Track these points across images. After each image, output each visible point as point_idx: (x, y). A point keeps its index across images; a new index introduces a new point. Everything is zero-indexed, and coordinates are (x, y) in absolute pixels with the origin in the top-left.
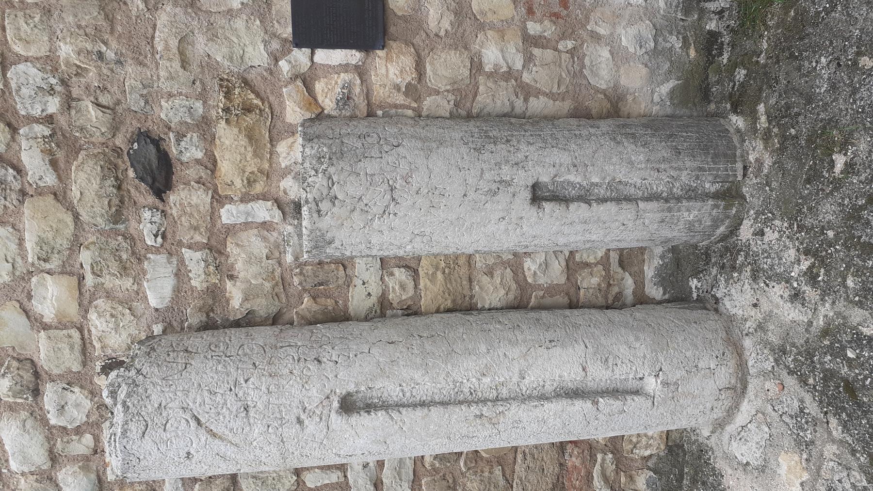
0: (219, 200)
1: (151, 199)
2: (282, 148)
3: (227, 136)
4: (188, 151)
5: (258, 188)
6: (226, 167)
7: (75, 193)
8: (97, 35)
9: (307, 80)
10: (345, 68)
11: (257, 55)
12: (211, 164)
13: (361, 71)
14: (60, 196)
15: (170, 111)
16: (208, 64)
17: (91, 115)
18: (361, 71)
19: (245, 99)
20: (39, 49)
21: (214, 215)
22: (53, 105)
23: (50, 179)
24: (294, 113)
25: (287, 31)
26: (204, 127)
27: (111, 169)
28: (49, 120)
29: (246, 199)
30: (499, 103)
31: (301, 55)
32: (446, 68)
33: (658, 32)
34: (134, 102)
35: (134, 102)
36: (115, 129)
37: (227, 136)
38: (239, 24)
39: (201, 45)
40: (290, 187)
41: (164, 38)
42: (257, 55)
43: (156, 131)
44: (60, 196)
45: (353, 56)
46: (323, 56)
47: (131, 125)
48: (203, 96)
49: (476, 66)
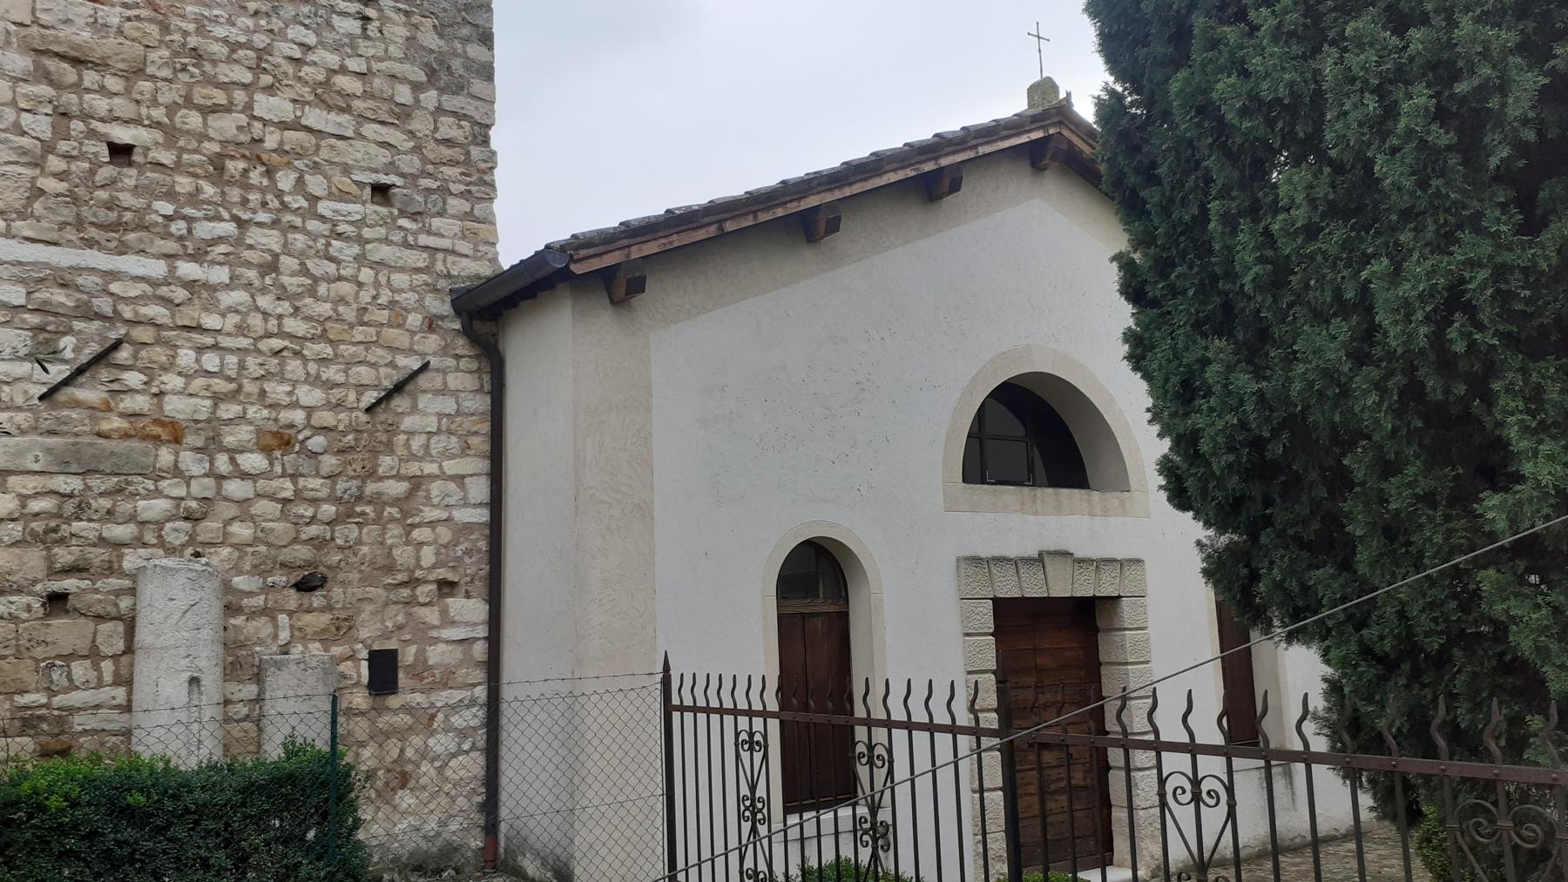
0: (291, 614)
1: (293, 582)
2: (318, 645)
3: (325, 618)
4: (317, 599)
5: (297, 633)
6: (308, 618)
7: (298, 547)
8: (372, 563)
9: (352, 657)
10: (359, 676)
11: (364, 634)
12: (309, 611)
13: (357, 684)
14: (296, 540)
15: (337, 592)
16: (359, 611)
17: (335, 558)
18: (357, 684)
19: (343, 627)
20: (365, 538)
21: (283, 611)
22: (340, 542)
23: (304, 537)
24: (337, 650)
25: (376, 647)
26: (329, 608)
27: (309, 564)
28: (333, 539)
29: (292, 627)
30: (475, 722)
31: (364, 654)
32: (360, 728)
33: (382, 845)
34: (341, 577)
35: (341, 577)
36: (327, 567)
37: (325, 618)
38: (379, 625)
39: (369, 608)
40: (297, 650)
41: (372, 591)
42: (364, 634)
43: (327, 585)
44: (296, 540)
45: (365, 680)
46: (365, 664)
47: (330, 575)
48: (344, 608)
49: (362, 745)
